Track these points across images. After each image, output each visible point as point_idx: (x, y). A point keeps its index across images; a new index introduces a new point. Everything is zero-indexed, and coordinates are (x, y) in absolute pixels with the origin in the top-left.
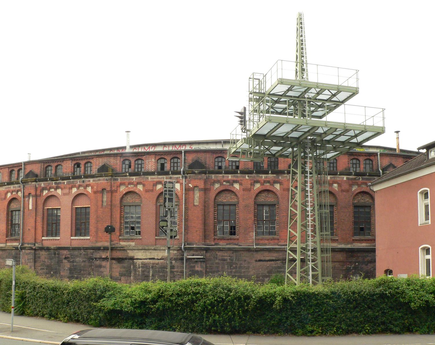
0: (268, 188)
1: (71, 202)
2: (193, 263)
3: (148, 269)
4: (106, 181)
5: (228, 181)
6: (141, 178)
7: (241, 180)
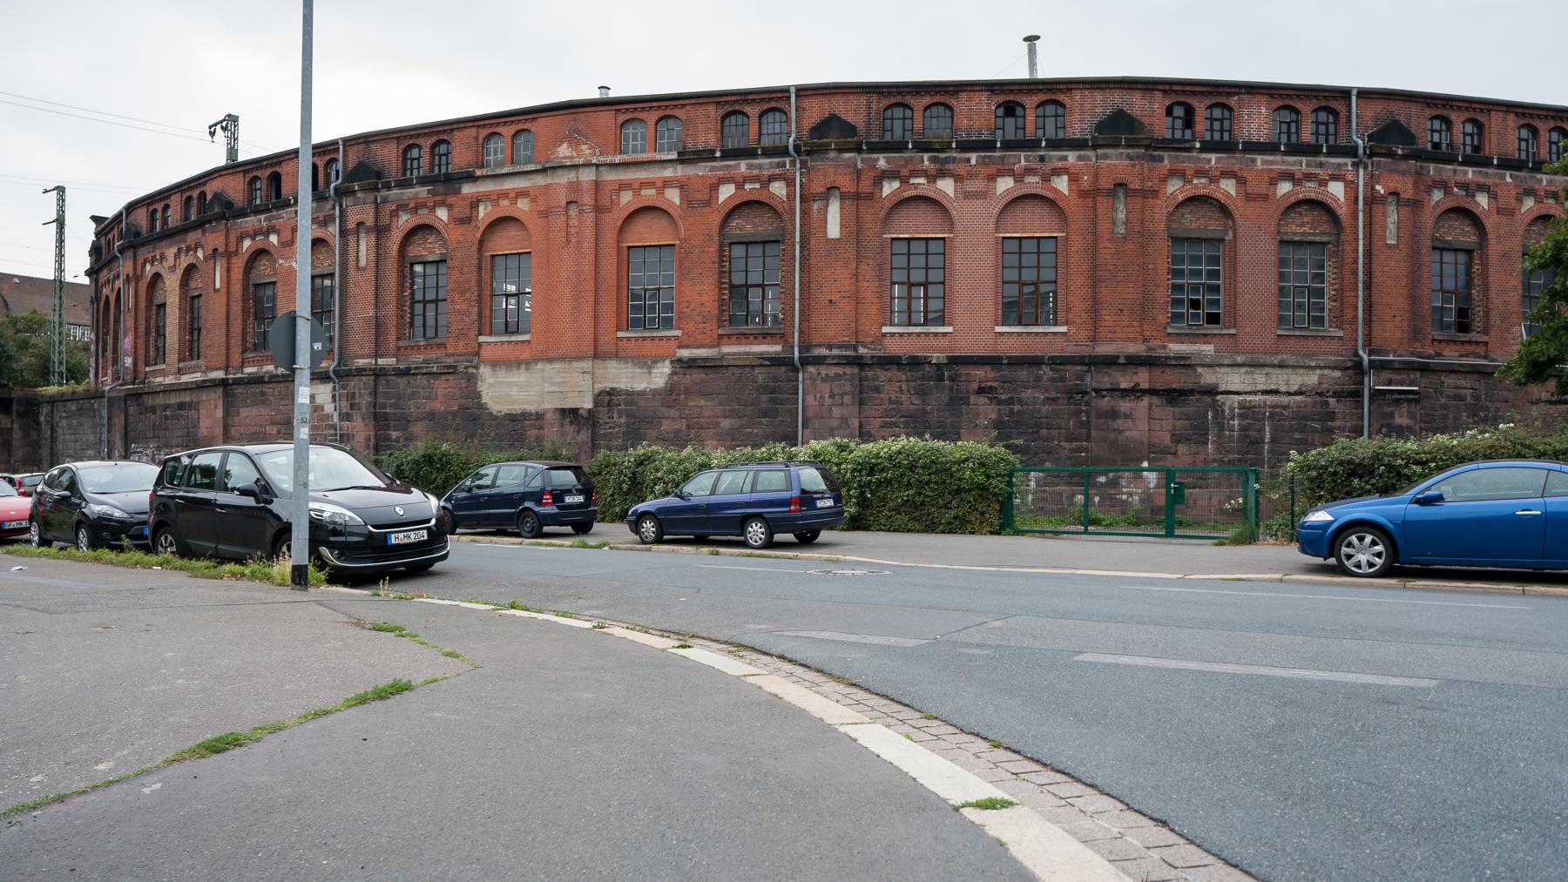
1: (993, 220)
2: (1389, 405)
3: (1258, 423)
4: (1126, 162)
5: (1465, 186)
6: (1234, 161)
7: (1496, 185)
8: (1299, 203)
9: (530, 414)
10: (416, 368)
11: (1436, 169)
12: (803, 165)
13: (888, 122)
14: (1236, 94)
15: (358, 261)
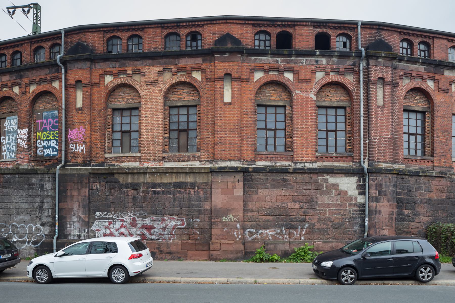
0: (276, 79)
10: (422, 172)
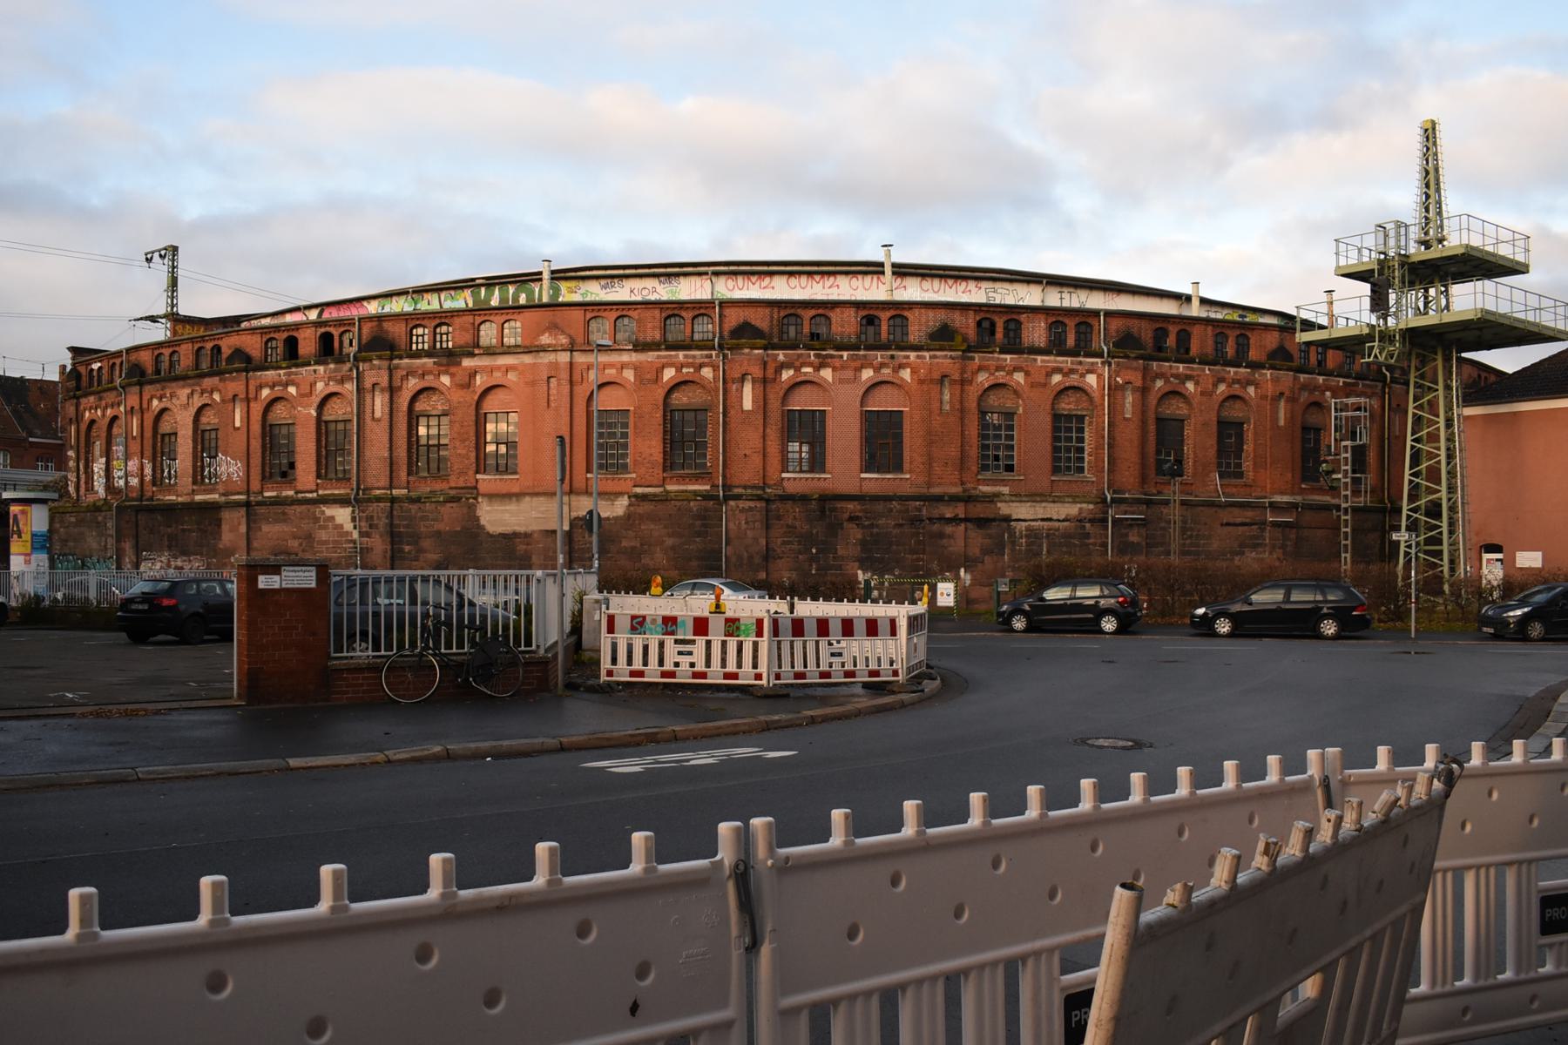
0: (1237, 393)
1: (859, 399)
5: (1177, 376)
7: (1199, 376)
8: (1067, 389)
9: (520, 533)
10: (425, 498)
11: (1158, 366)
12: (725, 356)
13: (785, 327)
14: (1024, 313)
15: (373, 413)
